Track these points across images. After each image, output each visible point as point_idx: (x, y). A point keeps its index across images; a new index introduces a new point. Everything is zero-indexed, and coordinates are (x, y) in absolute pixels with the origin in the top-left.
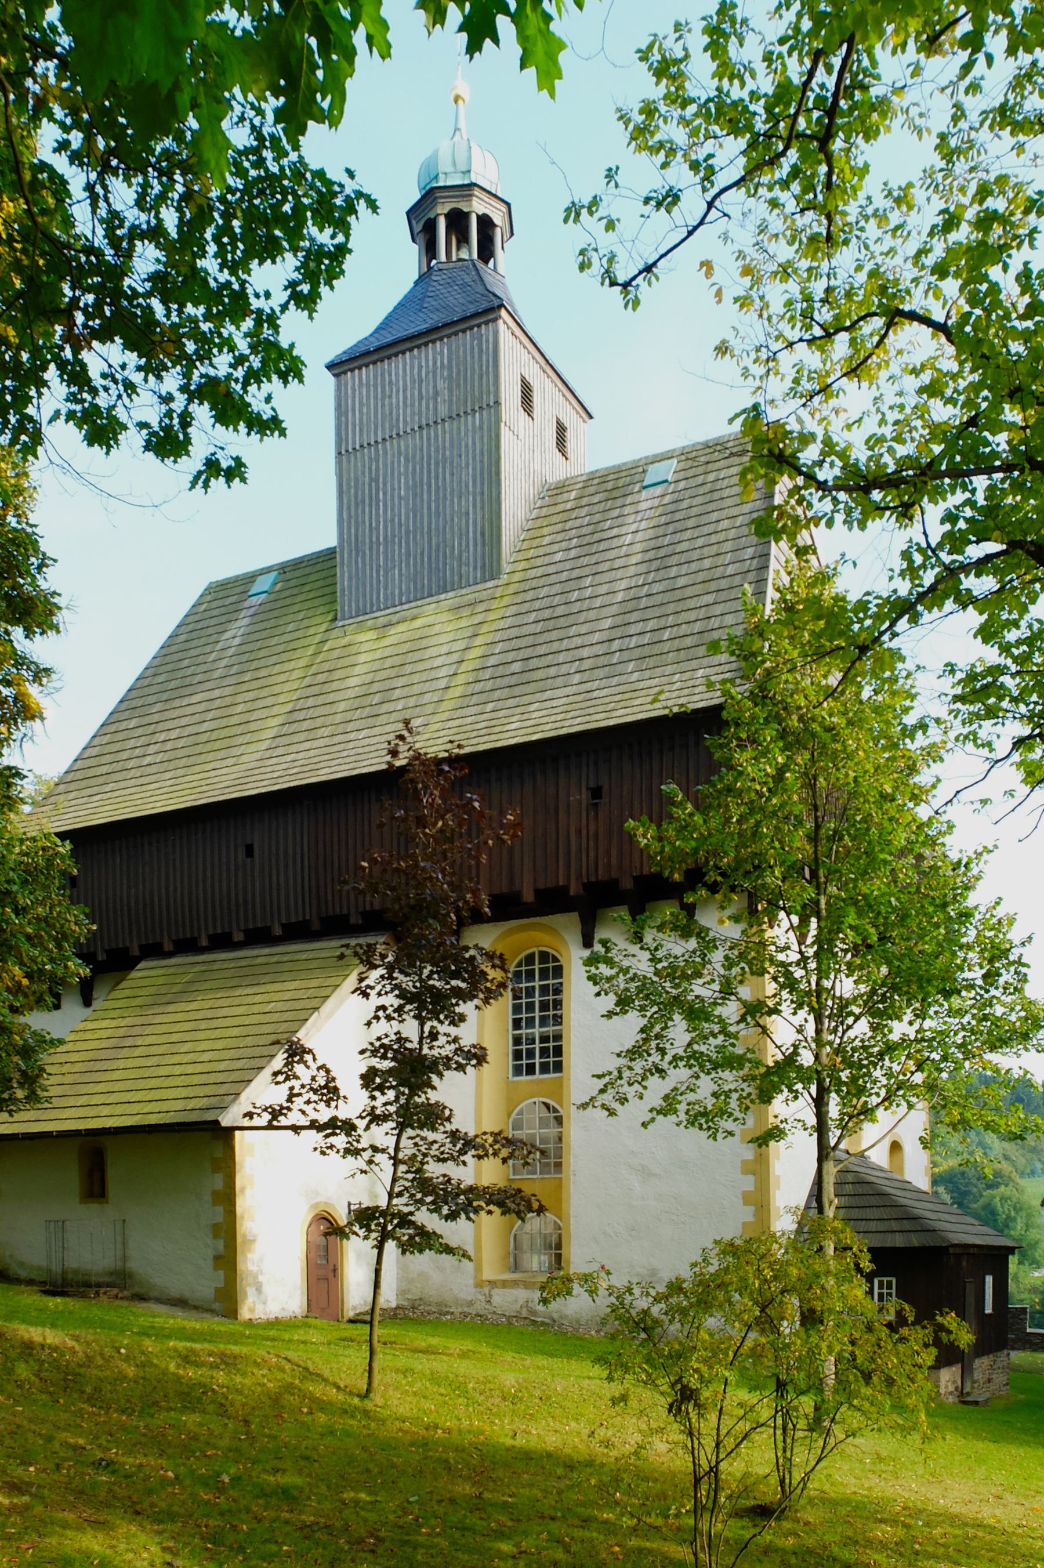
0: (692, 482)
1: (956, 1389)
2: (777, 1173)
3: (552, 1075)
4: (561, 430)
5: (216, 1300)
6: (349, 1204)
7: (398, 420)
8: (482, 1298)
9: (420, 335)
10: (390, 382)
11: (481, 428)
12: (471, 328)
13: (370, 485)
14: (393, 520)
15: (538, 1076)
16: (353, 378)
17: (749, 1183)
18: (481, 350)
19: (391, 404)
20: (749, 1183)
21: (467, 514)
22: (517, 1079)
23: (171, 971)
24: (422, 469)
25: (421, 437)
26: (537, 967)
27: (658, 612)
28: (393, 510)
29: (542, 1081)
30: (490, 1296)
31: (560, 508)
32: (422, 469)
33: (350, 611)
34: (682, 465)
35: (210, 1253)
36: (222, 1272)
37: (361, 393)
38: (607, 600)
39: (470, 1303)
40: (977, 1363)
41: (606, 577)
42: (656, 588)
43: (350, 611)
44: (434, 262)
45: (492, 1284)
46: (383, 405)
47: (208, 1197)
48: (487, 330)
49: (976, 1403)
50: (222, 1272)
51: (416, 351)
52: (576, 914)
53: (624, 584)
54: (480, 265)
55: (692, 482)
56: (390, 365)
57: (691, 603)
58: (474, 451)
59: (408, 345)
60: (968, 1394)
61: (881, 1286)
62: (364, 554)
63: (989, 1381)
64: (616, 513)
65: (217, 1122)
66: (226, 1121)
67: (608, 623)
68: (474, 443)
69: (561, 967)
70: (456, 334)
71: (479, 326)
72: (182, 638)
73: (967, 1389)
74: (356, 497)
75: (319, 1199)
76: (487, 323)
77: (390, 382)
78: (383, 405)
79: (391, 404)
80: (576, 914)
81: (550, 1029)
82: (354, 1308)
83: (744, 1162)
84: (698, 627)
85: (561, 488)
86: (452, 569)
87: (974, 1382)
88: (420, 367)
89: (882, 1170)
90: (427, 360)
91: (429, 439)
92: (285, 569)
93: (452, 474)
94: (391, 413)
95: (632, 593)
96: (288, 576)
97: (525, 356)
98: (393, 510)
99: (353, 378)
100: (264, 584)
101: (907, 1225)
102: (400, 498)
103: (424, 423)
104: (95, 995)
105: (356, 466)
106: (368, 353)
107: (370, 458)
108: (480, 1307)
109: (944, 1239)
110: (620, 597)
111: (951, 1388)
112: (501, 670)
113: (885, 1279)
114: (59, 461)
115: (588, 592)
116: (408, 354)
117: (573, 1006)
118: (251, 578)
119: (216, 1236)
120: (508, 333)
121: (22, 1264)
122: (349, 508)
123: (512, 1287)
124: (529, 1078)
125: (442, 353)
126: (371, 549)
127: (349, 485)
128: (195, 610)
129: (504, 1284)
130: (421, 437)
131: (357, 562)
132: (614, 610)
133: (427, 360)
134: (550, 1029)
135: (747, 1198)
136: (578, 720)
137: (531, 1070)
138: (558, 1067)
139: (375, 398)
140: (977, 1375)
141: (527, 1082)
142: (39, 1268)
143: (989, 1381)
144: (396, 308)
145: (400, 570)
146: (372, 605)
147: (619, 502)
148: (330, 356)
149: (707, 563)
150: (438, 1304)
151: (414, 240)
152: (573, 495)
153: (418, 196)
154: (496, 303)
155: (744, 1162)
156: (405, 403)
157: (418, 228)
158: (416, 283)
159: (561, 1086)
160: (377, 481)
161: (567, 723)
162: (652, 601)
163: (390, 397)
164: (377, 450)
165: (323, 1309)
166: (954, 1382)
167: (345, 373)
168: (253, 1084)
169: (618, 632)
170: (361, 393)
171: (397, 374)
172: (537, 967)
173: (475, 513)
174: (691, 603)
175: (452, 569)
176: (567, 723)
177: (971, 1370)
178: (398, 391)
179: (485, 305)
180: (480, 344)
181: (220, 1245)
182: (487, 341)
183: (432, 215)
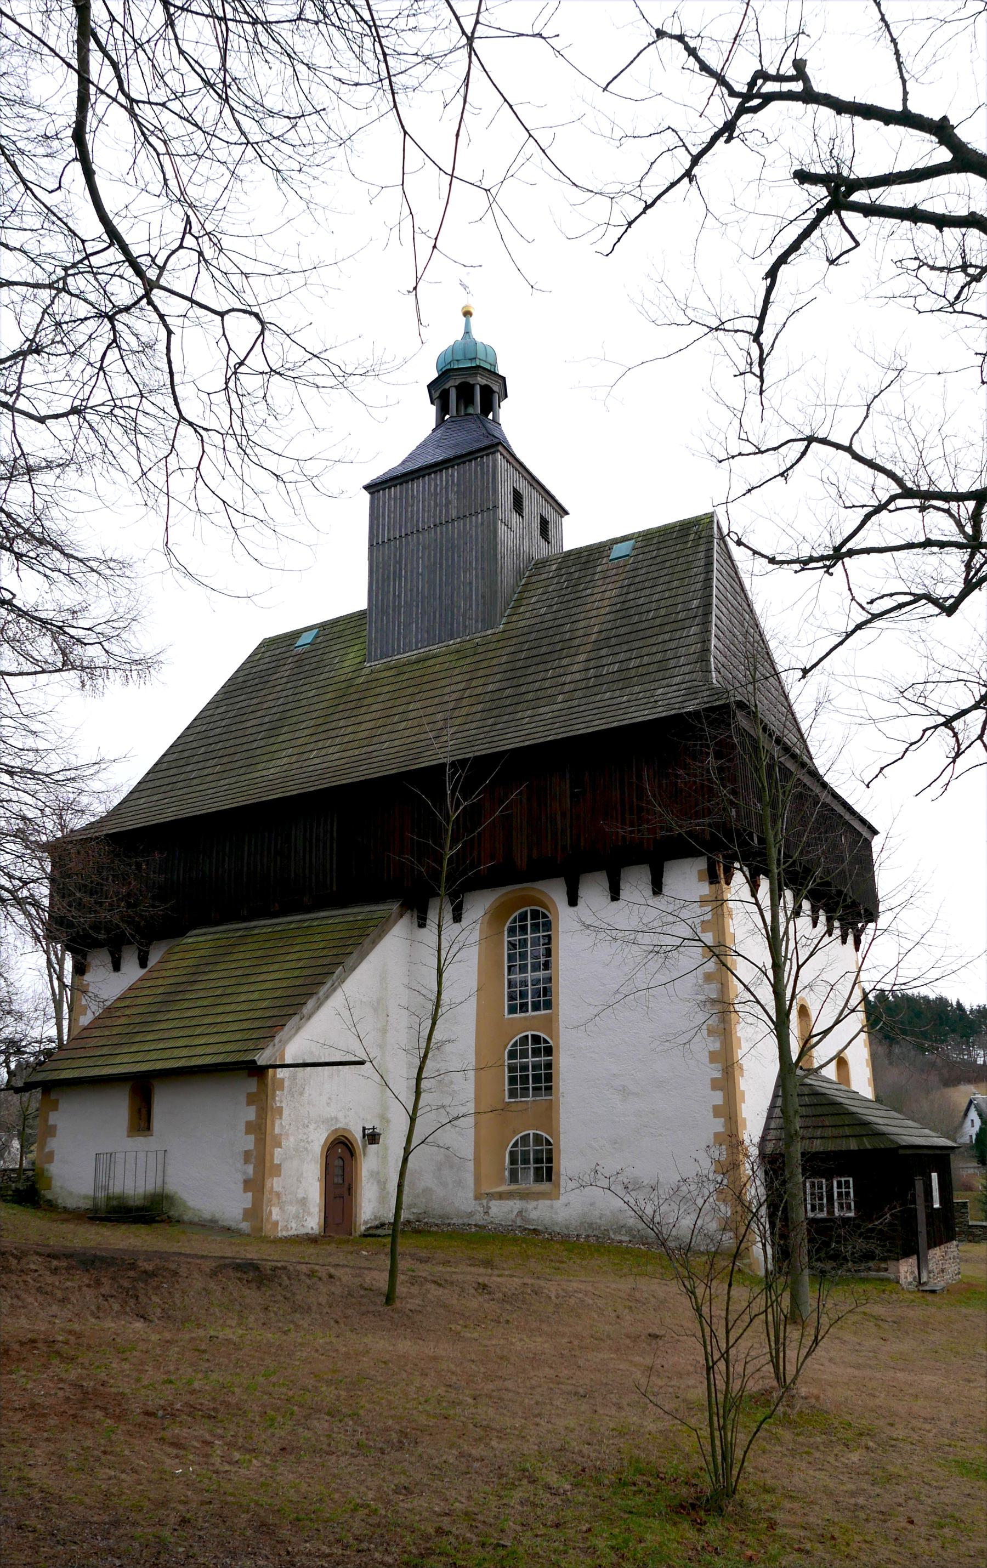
0: (649, 556)
1: (914, 1278)
2: (742, 1088)
3: (543, 1012)
4: (544, 523)
5: (244, 1219)
6: (364, 1129)
7: (418, 521)
8: (481, 1209)
9: (437, 464)
10: (413, 496)
11: (482, 524)
12: (476, 459)
13: (395, 566)
14: (411, 590)
15: (530, 1013)
16: (384, 495)
17: (718, 1098)
18: (483, 473)
19: (412, 511)
20: (718, 1098)
21: (471, 583)
22: (511, 1016)
23: (217, 936)
24: (435, 554)
25: (436, 533)
26: (529, 923)
27: (625, 647)
28: (412, 581)
29: (533, 1017)
30: (489, 1208)
31: (543, 576)
32: (435, 554)
33: (376, 655)
34: (639, 544)
35: (240, 1178)
36: (250, 1194)
37: (389, 504)
38: (585, 639)
39: (471, 1214)
40: (931, 1253)
41: (582, 624)
42: (623, 630)
43: (376, 655)
44: (447, 417)
45: (491, 1196)
46: (406, 512)
47: (242, 1127)
48: (488, 460)
49: (933, 1292)
50: (250, 1194)
51: (433, 475)
52: (604, 873)
53: (596, 629)
54: (482, 417)
55: (649, 556)
56: (413, 485)
57: (652, 641)
58: (477, 540)
59: (428, 471)
60: (925, 1283)
61: (839, 1186)
62: (388, 614)
63: (943, 1271)
64: (588, 579)
65: (254, 1062)
66: (262, 1059)
67: (582, 657)
68: (477, 534)
69: (550, 922)
70: (464, 463)
71: (482, 457)
72: (240, 680)
73: (924, 1279)
74: (383, 575)
75: (338, 1126)
76: (487, 455)
77: (413, 496)
78: (406, 512)
79: (412, 511)
80: (604, 873)
81: (517, 977)
82: (366, 1223)
83: (713, 1081)
84: (659, 657)
85: (542, 564)
86: (458, 623)
87: (929, 1272)
88: (436, 485)
89: (833, 1083)
90: (441, 481)
91: (441, 533)
92: (323, 626)
93: (459, 557)
94: (412, 517)
95: (603, 635)
96: (326, 632)
97: (516, 475)
98: (412, 581)
99: (384, 495)
100: (307, 638)
101: (858, 1130)
102: (418, 574)
103: (438, 521)
104: (622, 887)
105: (383, 554)
106: (397, 478)
107: (395, 547)
108: (479, 1218)
109: (892, 1141)
110: (594, 637)
111: (910, 1279)
112: (497, 695)
113: (843, 1179)
114: (177, 565)
115: (568, 636)
116: (427, 478)
117: (561, 953)
118: (296, 634)
119: (246, 1161)
120: (504, 463)
121: (71, 1193)
122: (377, 583)
123: (508, 1199)
124: (523, 1015)
125: (453, 475)
126: (394, 610)
127: (377, 566)
128: (252, 659)
129: (501, 1196)
130: (436, 533)
131: (382, 620)
132: (589, 647)
133: (441, 481)
134: (541, 974)
135: (717, 1112)
136: (562, 730)
137: (524, 1007)
138: (548, 1005)
139: (401, 507)
140: (932, 1265)
141: (521, 1018)
142: (86, 1197)
143: (943, 1271)
144: (418, 447)
145: (417, 624)
146: (393, 650)
147: (590, 571)
148: (367, 481)
149: (663, 612)
150: (440, 1217)
151: (432, 403)
152: (554, 567)
153: (437, 375)
154: (497, 441)
155: (713, 1081)
156: (423, 509)
157: (436, 395)
158: (434, 430)
159: (551, 1021)
160: (400, 563)
161: (553, 732)
162: (620, 640)
163: (412, 506)
164: (401, 543)
165: (338, 1225)
166: (912, 1273)
167: (378, 491)
168: (286, 1028)
169: (592, 664)
170: (389, 504)
171: (418, 491)
172: (529, 923)
173: (476, 582)
174: (652, 641)
175: (458, 623)
176: (553, 732)
177: (927, 1261)
178: (418, 502)
179: (486, 443)
180: (482, 469)
181: (250, 1169)
182: (488, 466)
183: (447, 387)
